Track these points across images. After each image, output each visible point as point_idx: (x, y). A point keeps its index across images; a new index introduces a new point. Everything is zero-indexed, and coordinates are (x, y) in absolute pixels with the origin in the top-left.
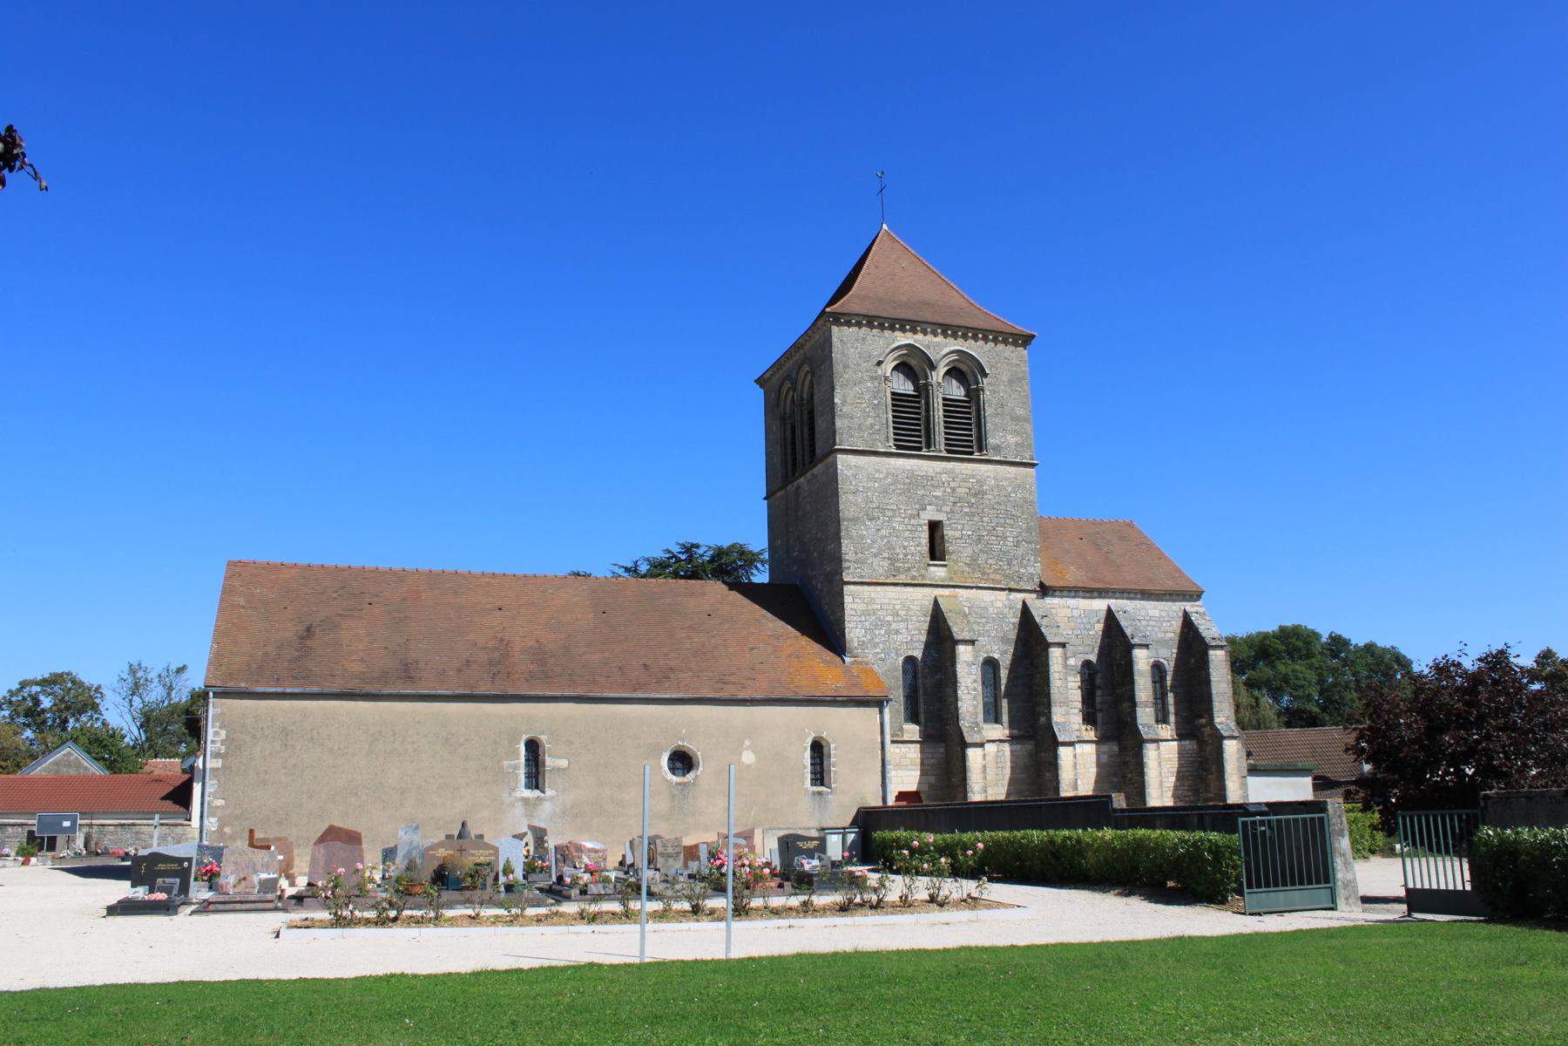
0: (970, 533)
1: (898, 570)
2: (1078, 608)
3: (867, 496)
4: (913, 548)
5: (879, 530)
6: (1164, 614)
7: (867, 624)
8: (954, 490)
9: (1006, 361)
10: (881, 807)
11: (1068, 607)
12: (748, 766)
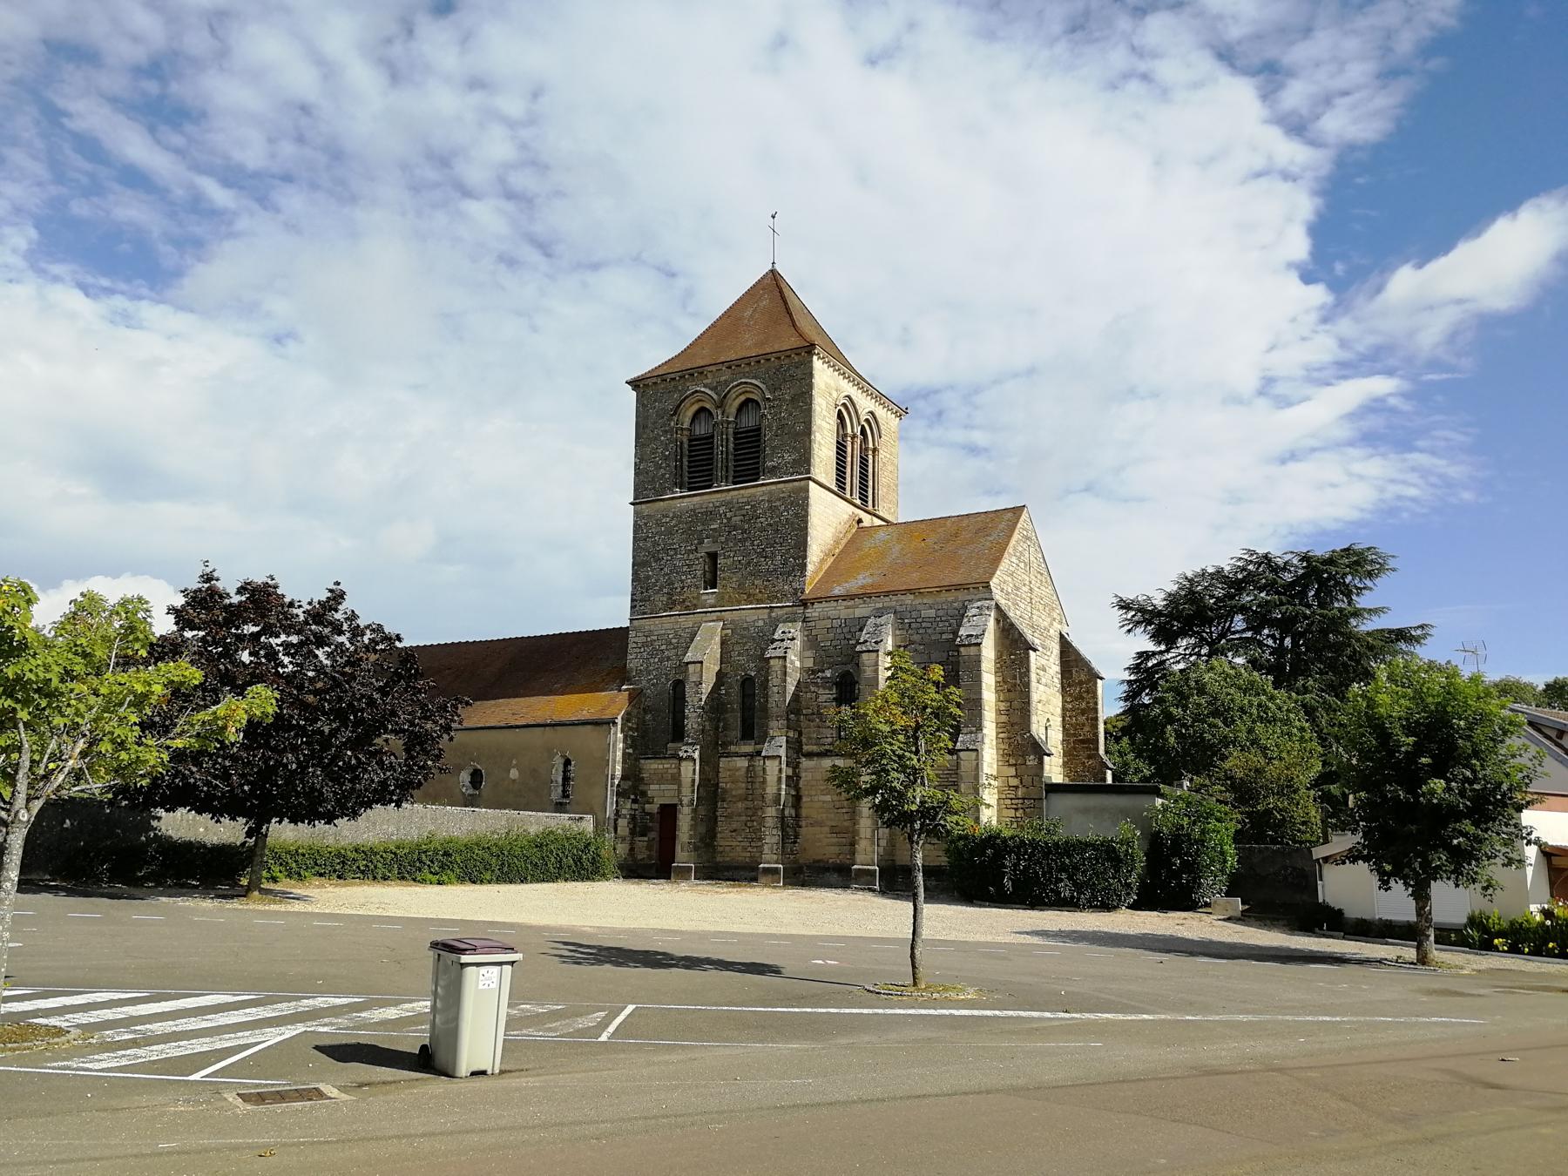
5: (662, 569)
6: (941, 613)
11: (829, 618)
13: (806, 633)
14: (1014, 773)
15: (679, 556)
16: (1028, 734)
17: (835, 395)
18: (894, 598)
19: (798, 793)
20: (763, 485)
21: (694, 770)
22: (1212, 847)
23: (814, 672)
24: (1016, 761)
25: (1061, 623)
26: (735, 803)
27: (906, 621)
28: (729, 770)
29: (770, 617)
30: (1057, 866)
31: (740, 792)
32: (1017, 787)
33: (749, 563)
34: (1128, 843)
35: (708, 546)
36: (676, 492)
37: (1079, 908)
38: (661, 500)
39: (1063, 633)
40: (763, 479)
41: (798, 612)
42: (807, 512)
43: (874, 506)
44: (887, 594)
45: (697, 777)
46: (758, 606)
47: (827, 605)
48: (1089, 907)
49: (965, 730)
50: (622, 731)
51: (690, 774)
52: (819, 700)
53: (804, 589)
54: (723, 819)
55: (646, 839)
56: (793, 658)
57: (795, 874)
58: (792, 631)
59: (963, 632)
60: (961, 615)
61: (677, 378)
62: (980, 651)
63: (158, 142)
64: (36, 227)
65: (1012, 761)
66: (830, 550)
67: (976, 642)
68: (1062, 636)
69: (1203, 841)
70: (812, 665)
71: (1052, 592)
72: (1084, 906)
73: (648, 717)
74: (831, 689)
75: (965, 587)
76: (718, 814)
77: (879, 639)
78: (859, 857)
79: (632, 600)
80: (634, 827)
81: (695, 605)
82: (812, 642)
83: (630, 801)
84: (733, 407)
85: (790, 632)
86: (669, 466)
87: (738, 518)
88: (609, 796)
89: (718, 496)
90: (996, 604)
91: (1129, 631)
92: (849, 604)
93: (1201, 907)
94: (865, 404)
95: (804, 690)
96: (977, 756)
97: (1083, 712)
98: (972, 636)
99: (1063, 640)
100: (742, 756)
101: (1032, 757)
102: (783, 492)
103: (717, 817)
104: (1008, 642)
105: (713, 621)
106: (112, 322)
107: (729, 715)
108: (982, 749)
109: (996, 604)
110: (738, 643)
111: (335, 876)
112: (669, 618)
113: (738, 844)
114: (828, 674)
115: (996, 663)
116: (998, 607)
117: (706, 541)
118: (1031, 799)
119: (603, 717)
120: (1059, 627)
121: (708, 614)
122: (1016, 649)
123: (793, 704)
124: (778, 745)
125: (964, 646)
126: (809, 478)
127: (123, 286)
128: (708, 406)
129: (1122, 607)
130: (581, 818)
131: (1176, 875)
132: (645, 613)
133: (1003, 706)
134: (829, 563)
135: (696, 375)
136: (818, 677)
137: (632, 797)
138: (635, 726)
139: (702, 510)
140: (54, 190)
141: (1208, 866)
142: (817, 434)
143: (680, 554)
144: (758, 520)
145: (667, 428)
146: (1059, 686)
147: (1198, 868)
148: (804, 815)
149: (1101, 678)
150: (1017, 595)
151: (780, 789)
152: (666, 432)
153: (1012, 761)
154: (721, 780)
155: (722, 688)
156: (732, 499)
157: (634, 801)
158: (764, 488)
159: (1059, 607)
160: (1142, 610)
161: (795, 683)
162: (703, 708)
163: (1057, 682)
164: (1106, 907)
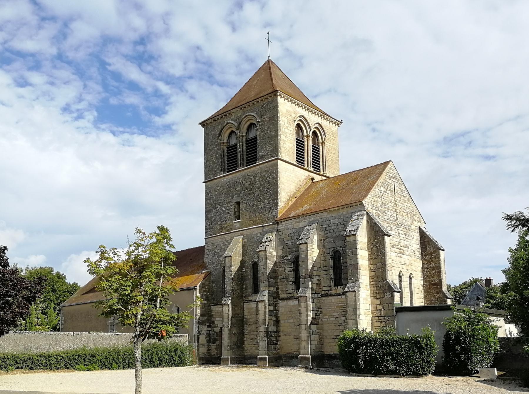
2: (293, 229)
3: (214, 199)
5: (217, 213)
6: (340, 220)
8: (244, 185)
11: (289, 229)
13: (279, 238)
14: (379, 303)
15: (224, 205)
16: (385, 281)
17: (293, 115)
18: (318, 215)
19: (277, 319)
20: (257, 165)
21: (229, 310)
22: (480, 339)
23: (283, 257)
24: (380, 296)
25: (420, 222)
26: (251, 325)
27: (324, 226)
28: (249, 309)
29: (263, 231)
30: (387, 353)
31: (253, 319)
32: (381, 310)
33: (253, 205)
34: (428, 338)
35: (236, 199)
36: (222, 174)
37: (400, 375)
38: (216, 179)
39: (421, 227)
40: (258, 162)
41: (275, 227)
42: (277, 176)
43: (323, 172)
44: (314, 213)
45: (230, 313)
46: (258, 226)
47: (287, 222)
48: (407, 375)
49: (350, 281)
50: (200, 292)
51: (227, 312)
52: (286, 271)
53: (277, 215)
54: (247, 333)
55: (215, 345)
56: (271, 250)
57: (276, 360)
58: (271, 237)
59: (348, 229)
60: (348, 220)
61: (220, 118)
62: (356, 238)
63: (142, 71)
64: (97, 111)
65: (378, 296)
66: (294, 195)
67: (353, 233)
68: (420, 229)
69: (474, 335)
70: (282, 254)
71: (413, 206)
72: (403, 374)
73: (214, 285)
74: (291, 265)
75: (351, 205)
76: (245, 331)
77: (308, 237)
78: (302, 351)
79: (206, 229)
80: (209, 339)
81: (231, 229)
82: (281, 242)
83: (206, 326)
84: (244, 127)
85: (269, 238)
86: (218, 162)
87: (248, 183)
88: (194, 324)
89: (239, 173)
90: (367, 213)
91: (513, 231)
92: (297, 220)
93: (475, 373)
94: (313, 119)
95: (279, 266)
96: (355, 294)
97: (433, 269)
98: (352, 230)
99: (421, 231)
100: (253, 302)
101: (388, 293)
102: (267, 167)
103: (244, 333)
104: (373, 232)
105: (239, 236)
106: (123, 145)
107: (247, 282)
108: (359, 291)
109: (367, 213)
110: (249, 246)
111: (28, 368)
112: (220, 236)
113: (254, 345)
114: (289, 257)
115: (368, 244)
116: (368, 214)
117: (235, 196)
118: (388, 316)
119: (191, 286)
120: (419, 224)
121: (237, 233)
122: (377, 236)
123: (272, 274)
124: (264, 296)
125: (348, 236)
126: (278, 159)
127: (128, 130)
128: (234, 130)
129: (508, 219)
130: (181, 336)
131: (458, 356)
132: (211, 235)
133: (372, 267)
134: (293, 202)
135: (227, 115)
136: (285, 259)
137: (207, 324)
138: (207, 290)
139: (233, 182)
140: (104, 95)
141: (477, 350)
142: (282, 136)
143: (225, 204)
144: (257, 183)
145: (217, 144)
146: (419, 256)
147: (470, 351)
148: (282, 330)
149: (443, 250)
150: (385, 208)
151: (265, 317)
152: (216, 145)
153: (378, 296)
154: (245, 314)
155: (244, 268)
156: (245, 174)
157: (209, 326)
158: (258, 167)
159: (419, 214)
160: (518, 219)
161: (273, 263)
162: (233, 279)
163: (418, 253)
164: (416, 374)
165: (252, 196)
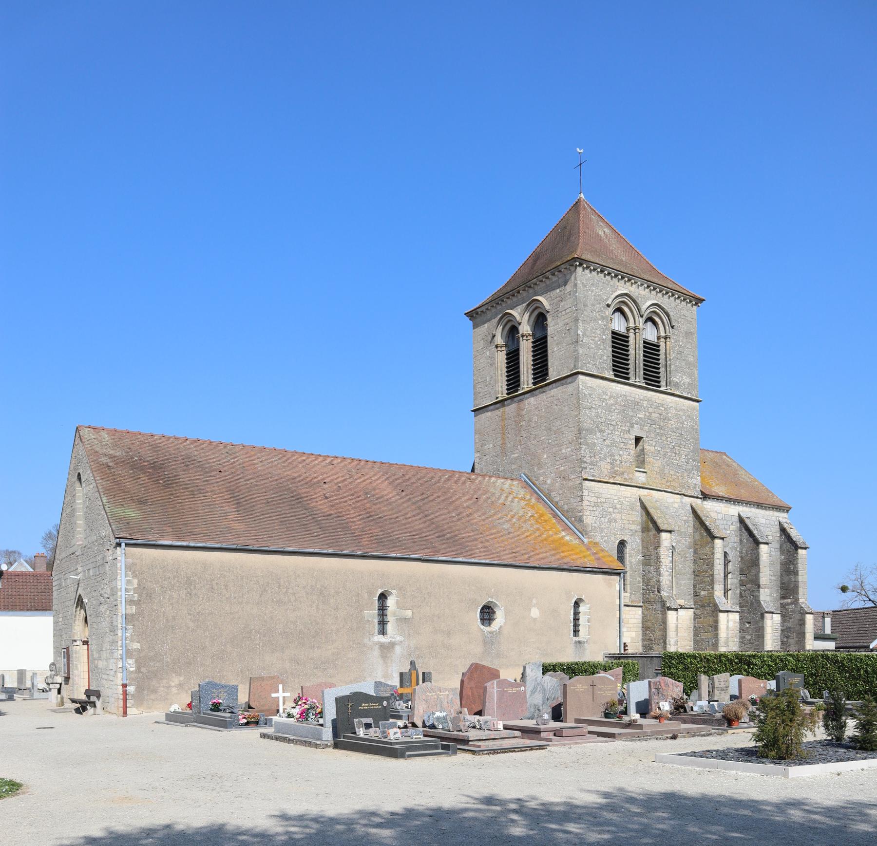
0: (659, 449)
1: (616, 473)
3: (598, 412)
4: (625, 456)
7: (597, 512)
9: (684, 317)
10: (618, 654)
11: (716, 512)
12: (535, 619)
15: (617, 433)
102: (684, 406)
165: (664, 438)
